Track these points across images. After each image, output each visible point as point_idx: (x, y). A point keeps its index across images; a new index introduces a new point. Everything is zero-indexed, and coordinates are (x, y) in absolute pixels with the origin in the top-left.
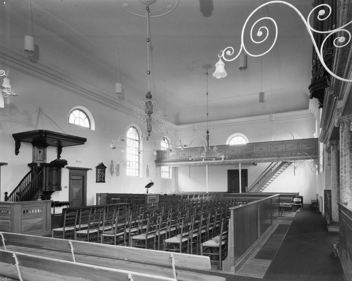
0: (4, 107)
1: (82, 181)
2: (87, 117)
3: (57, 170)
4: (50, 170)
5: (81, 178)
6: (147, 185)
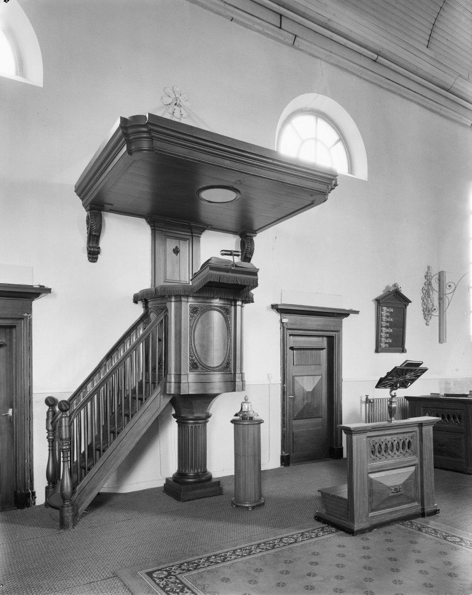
0: (44, 86)
1: (324, 353)
2: (343, 138)
3: (225, 312)
4: (194, 310)
5: (324, 342)
6: (389, 374)
